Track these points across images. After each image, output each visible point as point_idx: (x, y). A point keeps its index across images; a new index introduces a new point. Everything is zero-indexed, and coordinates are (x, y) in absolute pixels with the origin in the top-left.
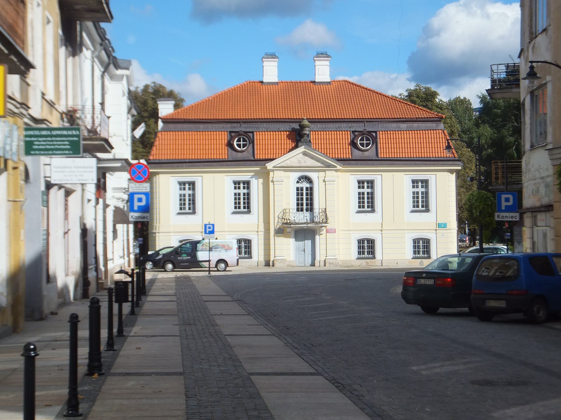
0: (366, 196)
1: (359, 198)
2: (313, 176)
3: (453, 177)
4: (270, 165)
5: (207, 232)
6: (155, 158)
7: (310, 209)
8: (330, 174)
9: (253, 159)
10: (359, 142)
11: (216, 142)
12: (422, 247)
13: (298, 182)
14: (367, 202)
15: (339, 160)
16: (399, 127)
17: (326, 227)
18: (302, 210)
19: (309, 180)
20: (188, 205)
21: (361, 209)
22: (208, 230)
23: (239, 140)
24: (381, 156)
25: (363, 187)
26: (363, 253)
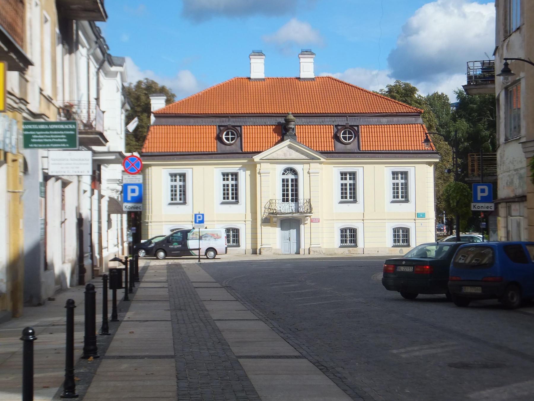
0: (348, 187)
1: (342, 189)
2: (298, 168)
3: (431, 169)
4: (257, 158)
5: (197, 222)
6: (147, 151)
7: (296, 199)
8: (314, 166)
9: (241, 152)
10: (341, 136)
11: (205, 135)
12: (402, 235)
13: (283, 174)
14: (349, 193)
15: (323, 153)
16: (380, 122)
17: (310, 216)
18: (287, 201)
19: (294, 172)
20: (179, 196)
21: (344, 200)
22: (198, 220)
23: (227, 134)
24: (363, 148)
25: (346, 179)
26: (346, 242)
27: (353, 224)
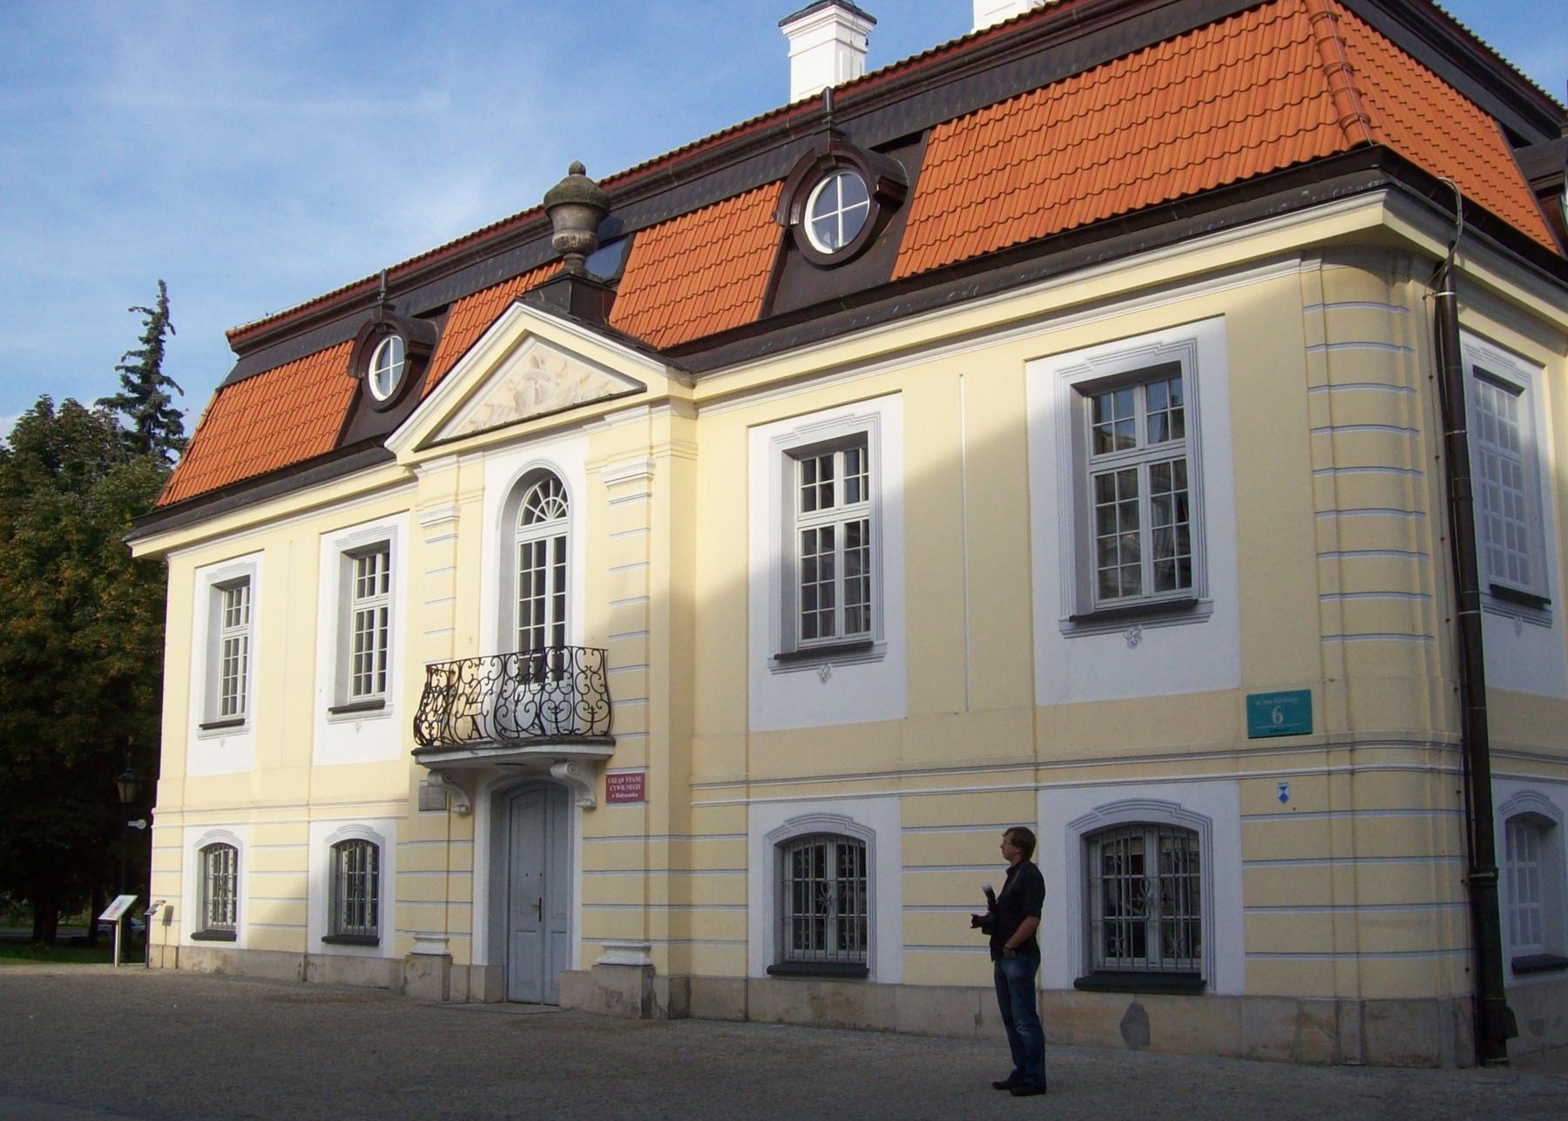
8: (638, 434)
27: (846, 808)
